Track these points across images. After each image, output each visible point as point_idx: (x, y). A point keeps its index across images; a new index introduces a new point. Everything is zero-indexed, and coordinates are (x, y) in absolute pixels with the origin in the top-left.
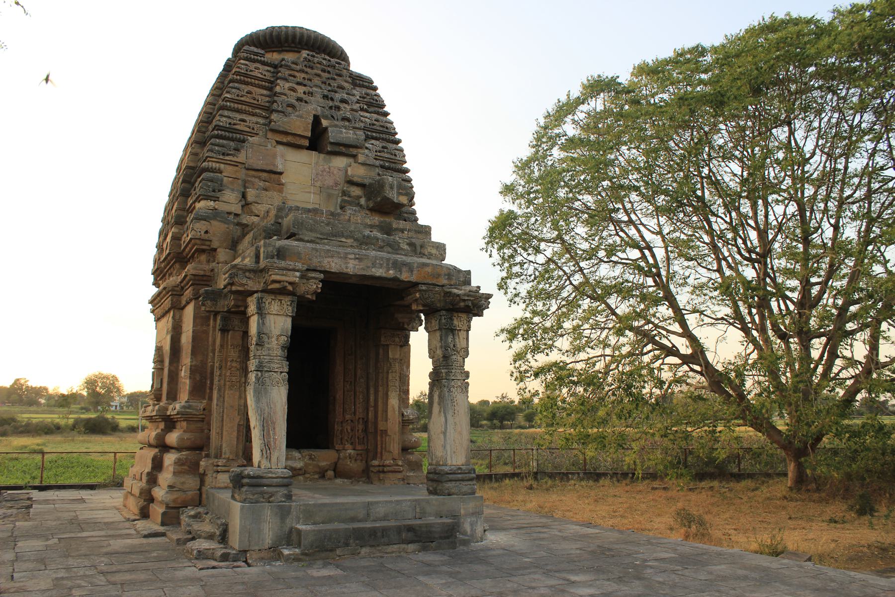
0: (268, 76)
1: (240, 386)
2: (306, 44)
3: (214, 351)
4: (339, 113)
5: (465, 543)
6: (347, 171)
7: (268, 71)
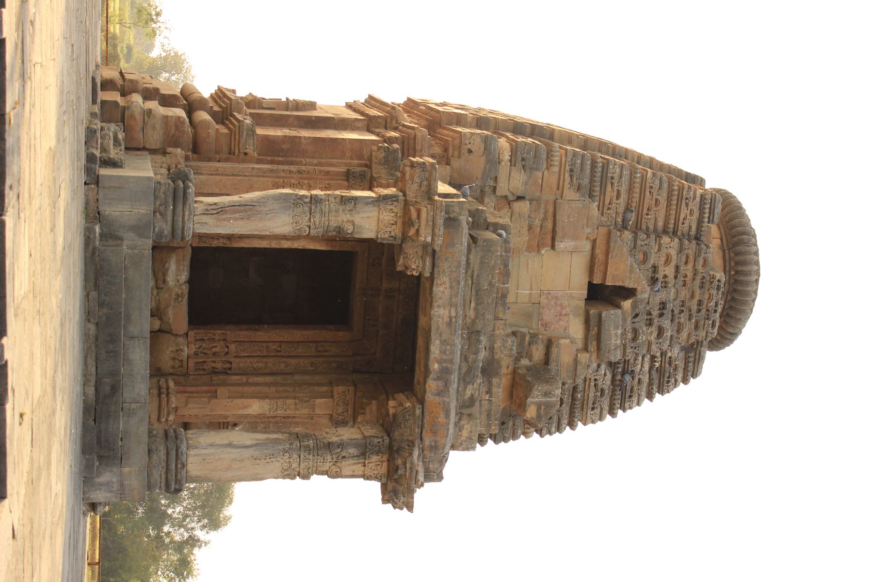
0: (683, 228)
3: (320, 164)
4: (642, 324)
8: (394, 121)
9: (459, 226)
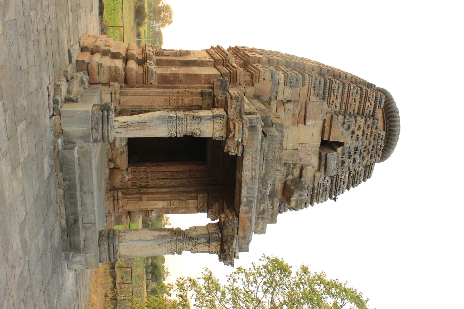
0: (367, 112)
1: (167, 106)
2: (389, 134)
3: (189, 88)
5: (67, 258)
6: (309, 165)
7: (370, 111)
8: (227, 62)
9: (257, 130)
